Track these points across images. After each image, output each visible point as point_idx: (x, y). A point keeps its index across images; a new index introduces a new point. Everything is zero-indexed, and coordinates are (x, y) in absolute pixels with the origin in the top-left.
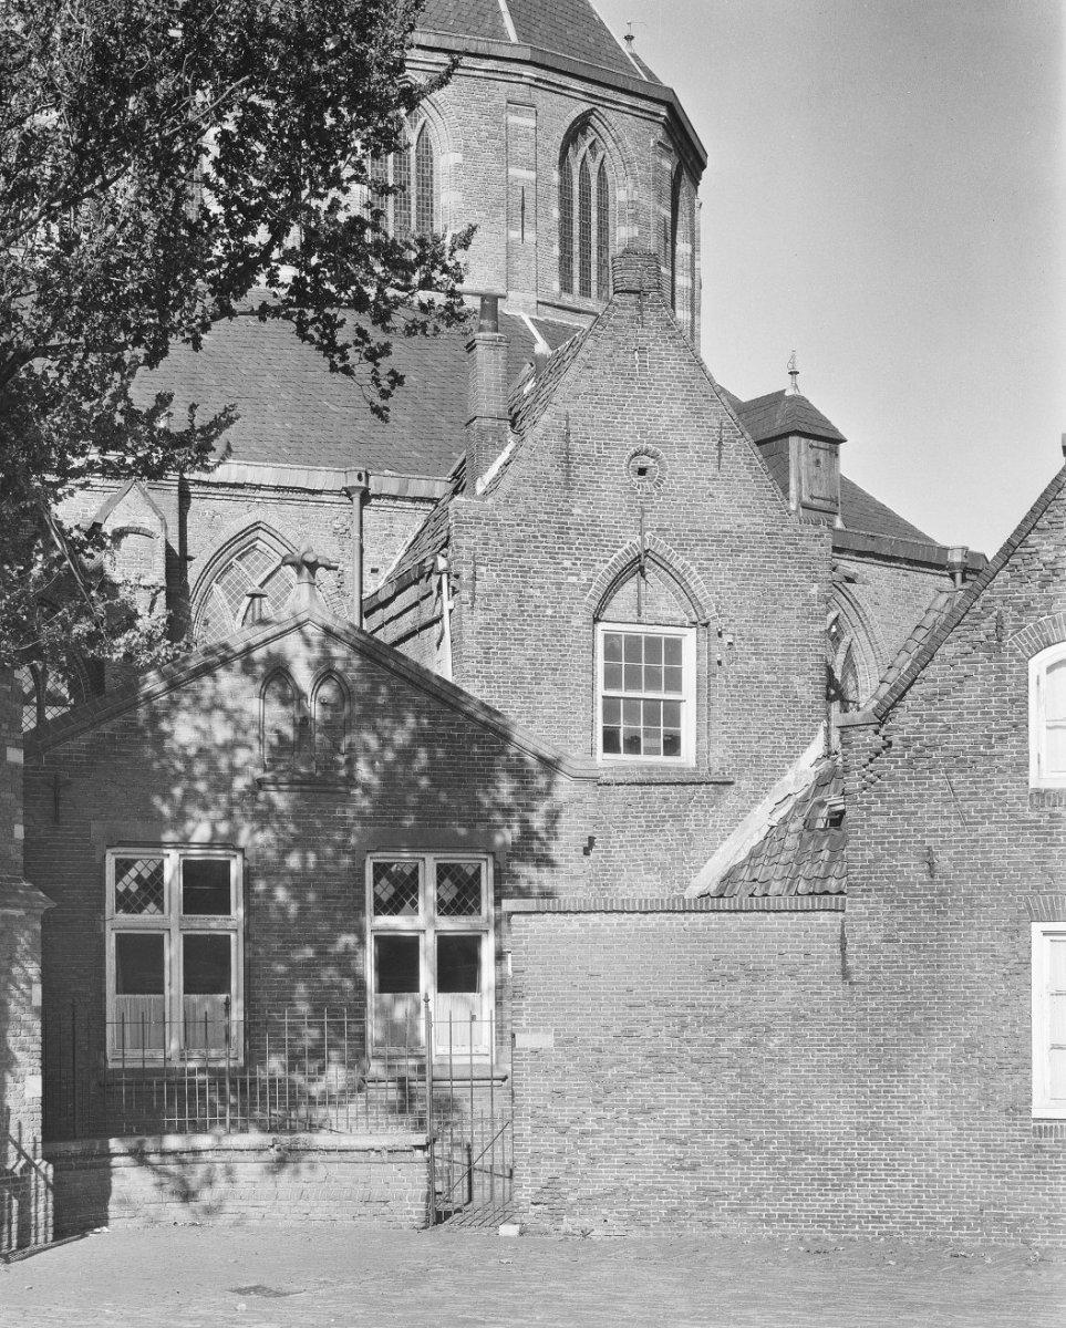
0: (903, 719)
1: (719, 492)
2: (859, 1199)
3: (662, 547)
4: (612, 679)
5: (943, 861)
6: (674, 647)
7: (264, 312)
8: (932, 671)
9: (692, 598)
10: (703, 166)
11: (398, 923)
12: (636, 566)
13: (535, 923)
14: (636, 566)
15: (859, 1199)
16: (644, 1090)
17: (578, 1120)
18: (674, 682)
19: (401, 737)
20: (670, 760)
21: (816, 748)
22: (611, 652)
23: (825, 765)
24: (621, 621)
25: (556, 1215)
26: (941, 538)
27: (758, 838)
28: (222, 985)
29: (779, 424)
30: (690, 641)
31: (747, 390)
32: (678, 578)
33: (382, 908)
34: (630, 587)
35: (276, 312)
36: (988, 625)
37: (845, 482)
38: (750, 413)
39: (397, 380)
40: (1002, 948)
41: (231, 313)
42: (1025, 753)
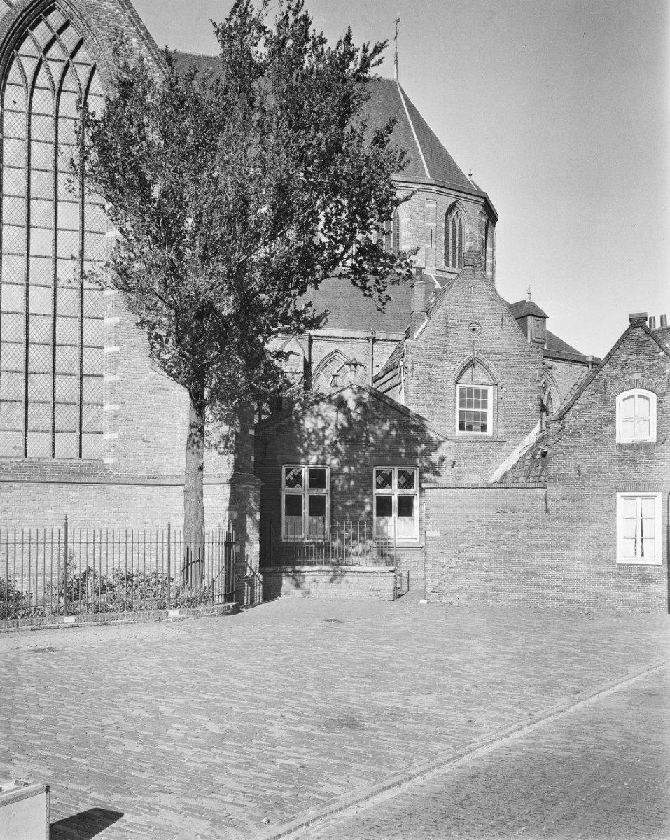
3: (481, 356)
4: (484, 416)
5: (584, 470)
6: (485, 393)
7: (340, 276)
12: (471, 364)
14: (471, 364)
15: (552, 592)
16: (473, 552)
17: (448, 563)
18: (485, 405)
21: (537, 429)
22: (462, 395)
24: (466, 383)
25: (440, 597)
29: (524, 312)
30: (491, 390)
32: (487, 368)
33: (379, 486)
34: (469, 371)
36: (601, 384)
42: (614, 431)
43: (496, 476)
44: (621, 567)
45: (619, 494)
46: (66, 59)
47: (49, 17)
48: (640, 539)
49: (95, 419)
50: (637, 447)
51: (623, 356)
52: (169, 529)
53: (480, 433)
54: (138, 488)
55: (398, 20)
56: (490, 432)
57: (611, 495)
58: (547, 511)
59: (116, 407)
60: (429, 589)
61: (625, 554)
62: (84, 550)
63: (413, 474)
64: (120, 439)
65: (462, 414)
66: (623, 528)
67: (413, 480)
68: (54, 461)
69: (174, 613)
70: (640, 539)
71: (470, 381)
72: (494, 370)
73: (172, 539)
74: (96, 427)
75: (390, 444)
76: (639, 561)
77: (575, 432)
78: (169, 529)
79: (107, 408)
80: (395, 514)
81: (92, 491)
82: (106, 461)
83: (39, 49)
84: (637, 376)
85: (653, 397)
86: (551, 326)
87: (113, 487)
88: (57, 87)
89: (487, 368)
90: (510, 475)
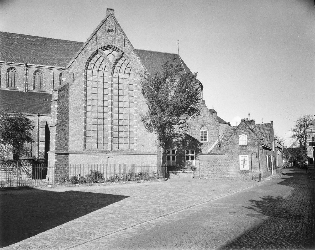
0: (229, 140)
1: (210, 119)
2: (227, 176)
3: (205, 124)
4: (206, 137)
5: (233, 151)
6: (206, 132)
7: (186, 113)
8: (231, 137)
9: (208, 128)
10: (203, 88)
11: (188, 155)
12: (203, 126)
13: (201, 155)
14: (203, 126)
15: (227, 176)
16: (210, 168)
17: (205, 170)
18: (206, 135)
19: (190, 141)
20: (206, 141)
21: (218, 140)
22: (201, 133)
23: (219, 141)
24: (202, 130)
25: (203, 177)
26: (226, 121)
27: (213, 148)
28: (175, 160)
29: (212, 112)
30: (207, 131)
31: (209, 109)
32: (207, 126)
33: (187, 154)
34: (203, 127)
35: (187, 113)
36: (236, 133)
37: (218, 116)
38: (211, 110)
39: (195, 118)
40: (237, 157)
41: (184, 114)
42: (239, 143)
43: (209, 151)
44: (241, 170)
45: (240, 156)
46: (126, 67)
47: (122, 58)
48: (244, 165)
49: (132, 141)
50: (243, 146)
51: (240, 128)
52: (102, 164)
53: (205, 141)
54: (142, 155)
55: (179, 40)
56: (207, 141)
57: (238, 156)
58: (225, 159)
59: (137, 138)
60: (201, 176)
61: (241, 168)
62: (119, 168)
63: (194, 151)
64: (138, 145)
65: (201, 137)
66: (241, 163)
67: (194, 152)
68: (124, 150)
69: (158, 180)
70: (244, 165)
71: (203, 130)
72: (208, 127)
73: (123, 168)
74: (132, 143)
75: (193, 145)
76: (244, 169)
77: (231, 143)
78: (102, 164)
79: (135, 139)
80: (194, 160)
81: (133, 156)
82: (135, 150)
83: (120, 65)
84: (243, 132)
85: (246, 136)
86: (218, 115)
87: (137, 155)
88: (124, 73)
89: (207, 126)
90: (212, 150)
